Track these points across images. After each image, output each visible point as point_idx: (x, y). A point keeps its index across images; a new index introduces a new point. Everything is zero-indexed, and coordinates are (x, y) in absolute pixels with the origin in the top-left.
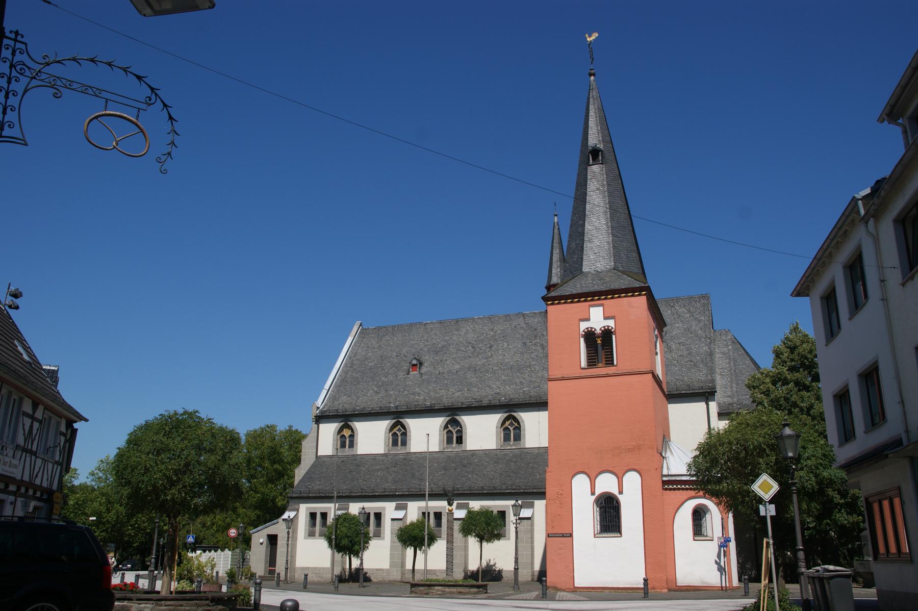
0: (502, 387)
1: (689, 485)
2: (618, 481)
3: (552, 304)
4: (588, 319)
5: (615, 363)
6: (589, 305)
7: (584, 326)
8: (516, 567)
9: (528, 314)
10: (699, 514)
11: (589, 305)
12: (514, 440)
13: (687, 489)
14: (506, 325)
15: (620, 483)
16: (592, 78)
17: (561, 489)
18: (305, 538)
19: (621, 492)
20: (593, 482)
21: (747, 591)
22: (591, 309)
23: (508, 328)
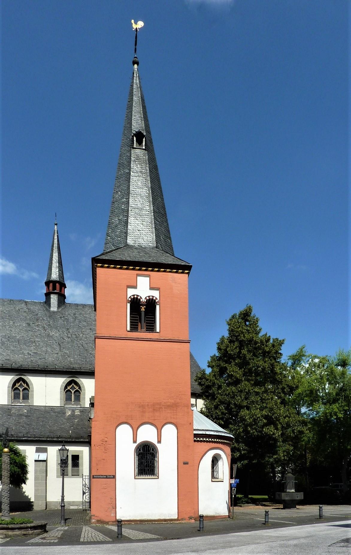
0: (12, 355)
1: (212, 439)
2: (158, 432)
3: (102, 267)
4: (135, 287)
5: (158, 330)
6: (137, 274)
7: (131, 292)
8: (63, 505)
9: (29, 302)
10: (215, 460)
11: (137, 274)
12: (23, 399)
13: (210, 442)
14: (11, 307)
16: (136, 66)
19: (159, 442)
20: (159, 431)
21: (267, 521)
22: (138, 278)
23: (12, 310)
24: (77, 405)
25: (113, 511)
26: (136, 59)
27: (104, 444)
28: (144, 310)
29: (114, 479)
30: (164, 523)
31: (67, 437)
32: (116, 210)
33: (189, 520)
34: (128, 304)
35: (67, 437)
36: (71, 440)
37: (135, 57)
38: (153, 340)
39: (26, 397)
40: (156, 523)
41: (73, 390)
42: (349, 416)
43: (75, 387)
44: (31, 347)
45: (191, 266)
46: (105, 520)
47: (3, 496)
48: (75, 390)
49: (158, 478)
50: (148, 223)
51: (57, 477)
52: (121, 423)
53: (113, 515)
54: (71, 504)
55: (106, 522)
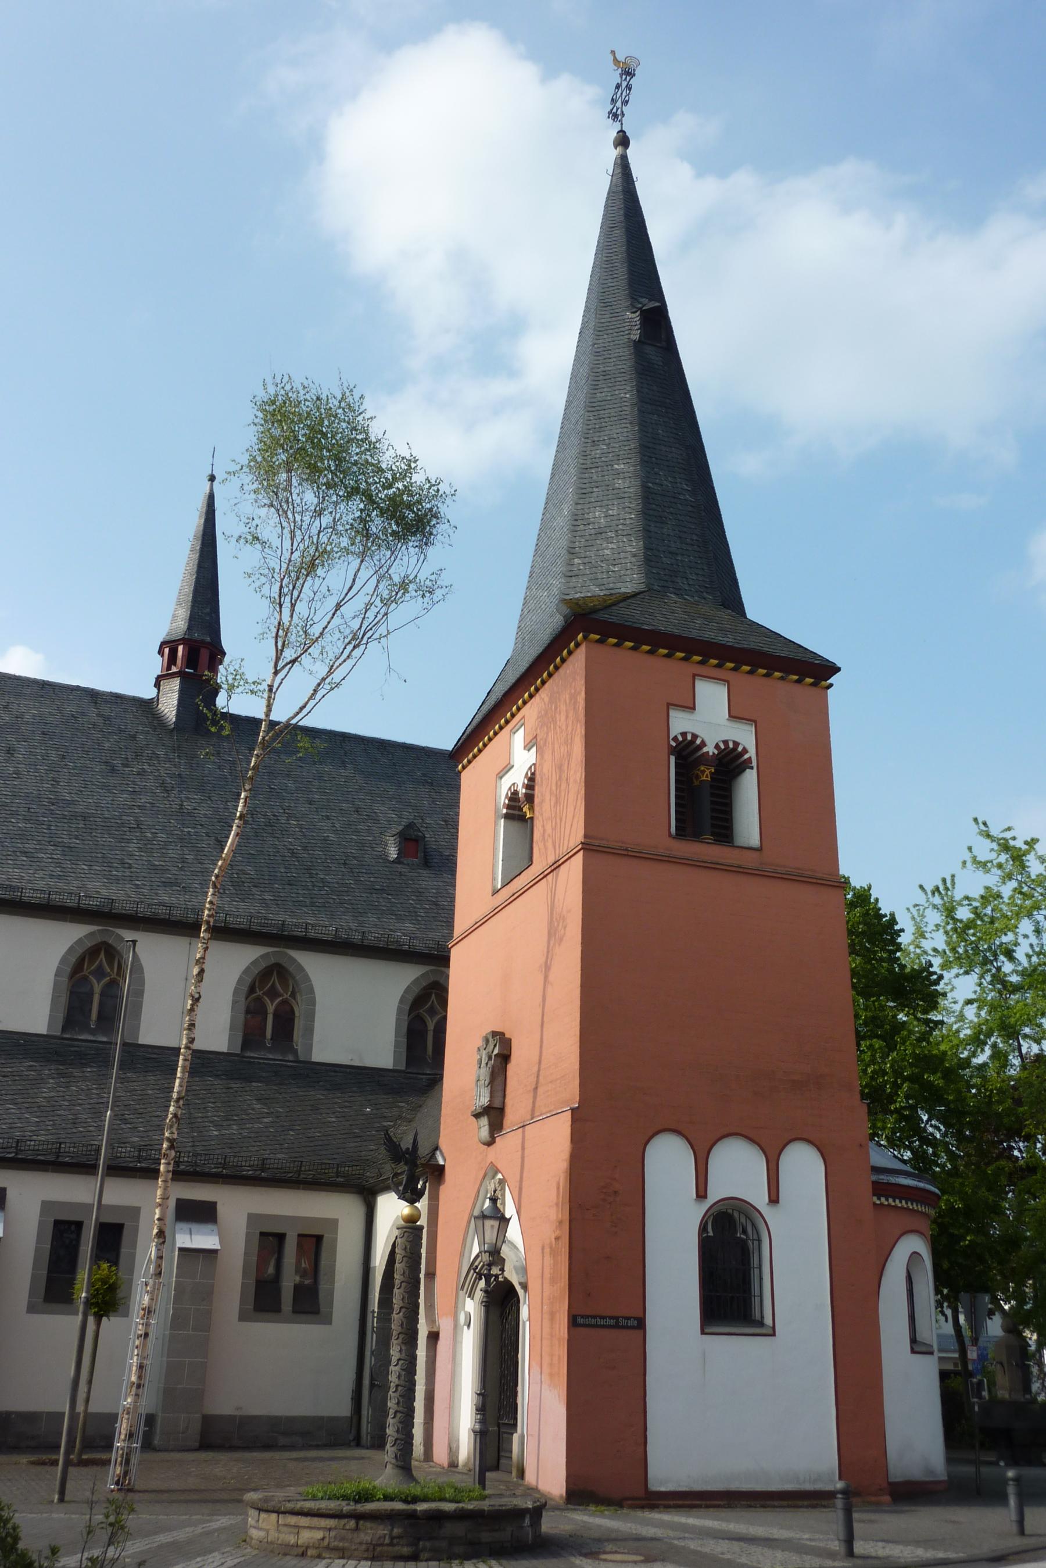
7: (680, 723)
18: (243, 1317)
19: (774, 1199)
27: (610, 1203)
28: (709, 779)
29: (638, 1333)
32: (595, 490)
34: (671, 756)
39: (108, 1019)
41: (272, 1002)
42: (898, 1134)
44: (129, 841)
45: (838, 669)
48: (281, 998)
50: (695, 538)
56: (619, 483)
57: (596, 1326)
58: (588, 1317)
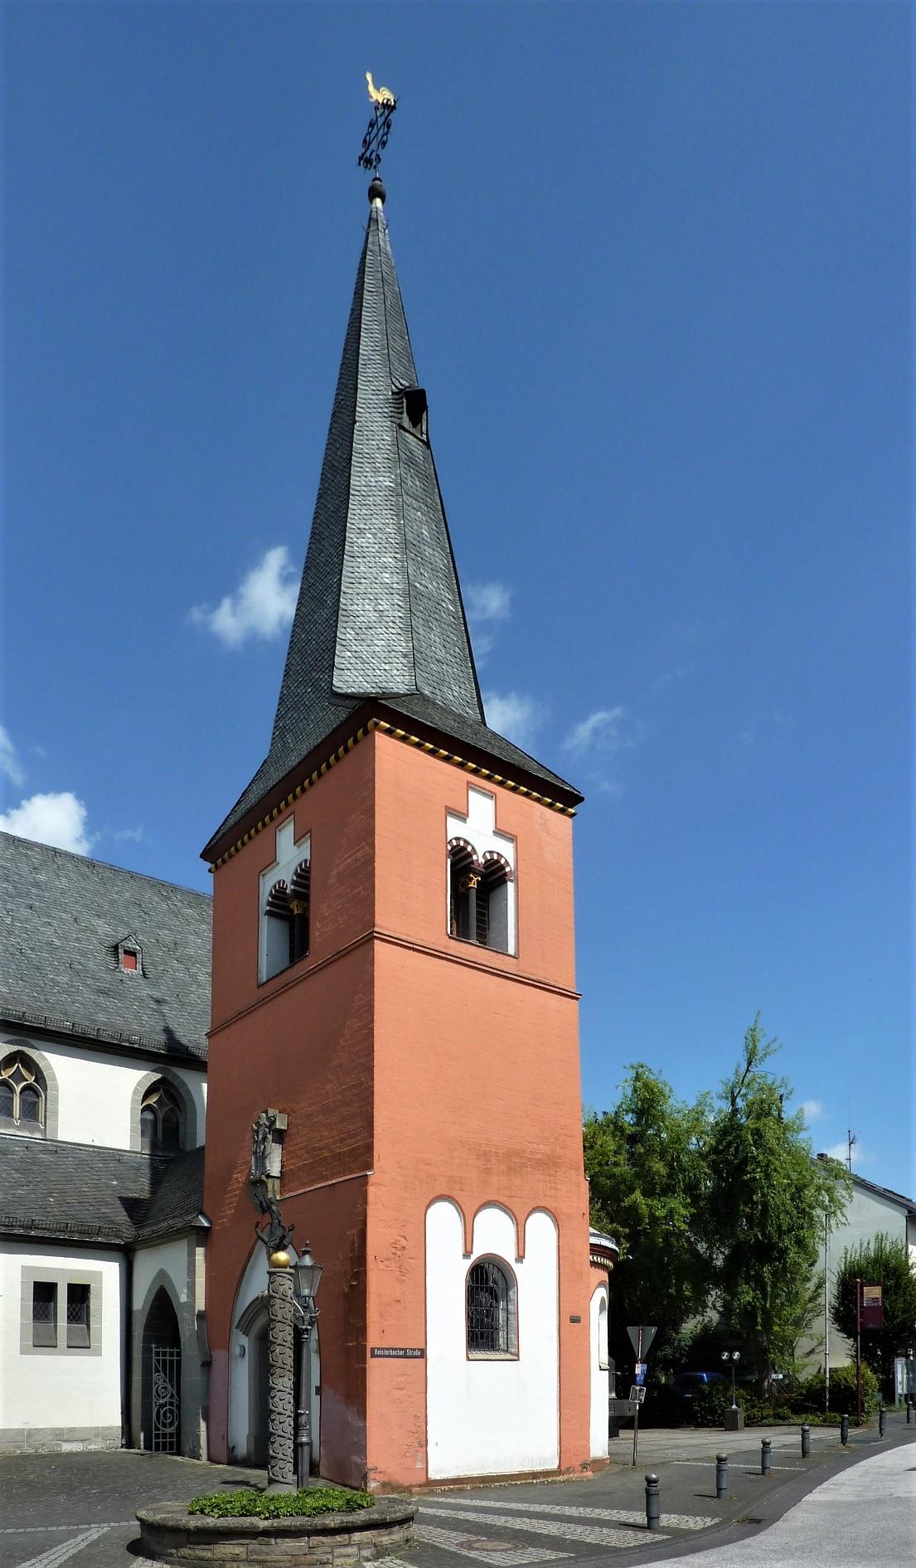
3: (389, 732)
4: (462, 816)
7: (455, 829)
11: (468, 783)
15: (521, 1234)
16: (378, 201)
17: (403, 1234)
19: (520, 1258)
24: (32, 1131)
25: (420, 1455)
26: (378, 182)
29: (423, 1360)
30: (519, 1483)
31: (26, 1223)
33: (582, 1472)
35: (26, 1223)
36: (67, 1237)
37: (376, 179)
38: (507, 975)
40: (519, 1483)
43: (22, 1075)
45: (582, 799)
46: (400, 1482)
47: (279, 1414)
48: (26, 1083)
49: (518, 1360)
51: (22, 1352)
52: (445, 1195)
53: (419, 1465)
54: (65, 1438)
55: (405, 1488)
56: (386, 577)
57: (389, 1356)
58: (383, 1349)
